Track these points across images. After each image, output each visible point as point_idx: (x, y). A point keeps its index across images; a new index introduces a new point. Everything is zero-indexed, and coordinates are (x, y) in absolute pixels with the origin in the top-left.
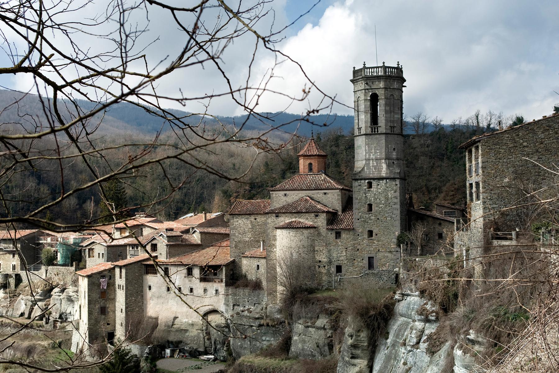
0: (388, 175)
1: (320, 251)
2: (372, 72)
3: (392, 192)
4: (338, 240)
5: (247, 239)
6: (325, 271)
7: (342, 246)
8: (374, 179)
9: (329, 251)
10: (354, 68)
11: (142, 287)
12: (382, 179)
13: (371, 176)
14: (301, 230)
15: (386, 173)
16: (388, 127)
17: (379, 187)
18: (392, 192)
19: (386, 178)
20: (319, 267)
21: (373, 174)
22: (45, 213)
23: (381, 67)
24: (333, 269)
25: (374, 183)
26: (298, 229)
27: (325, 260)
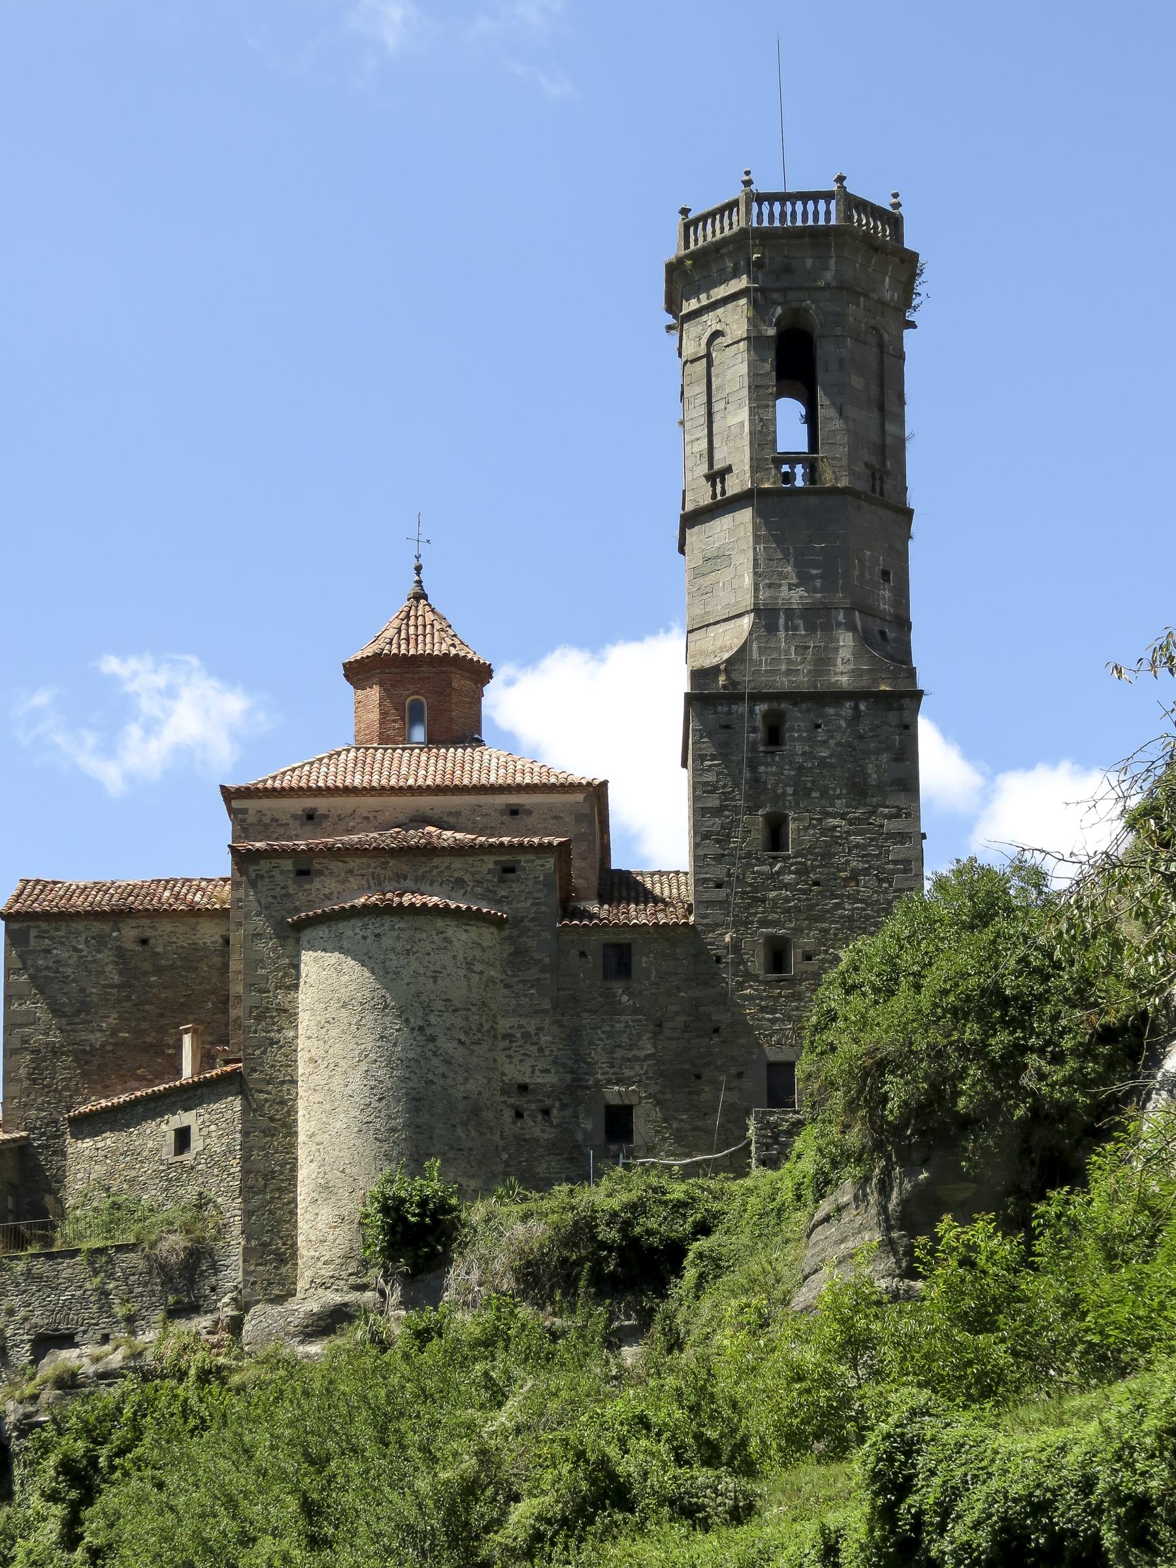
0: (864, 684)
1: (526, 1036)
2: (783, 215)
3: (885, 757)
4: (618, 987)
5: (97, 1039)
6: (549, 1134)
7: (635, 1011)
8: (795, 698)
9: (573, 1037)
10: (685, 211)
11: (695, 856)
12: (837, 697)
13: (783, 683)
14: (440, 923)
15: (856, 673)
16: (860, 468)
17: (821, 735)
18: (885, 757)
19: (854, 696)
20: (519, 1115)
21: (789, 672)
22: (599, 1169)
23: (828, 196)
24: (588, 1124)
25: (796, 724)
26: (421, 920)
27: (552, 1079)
